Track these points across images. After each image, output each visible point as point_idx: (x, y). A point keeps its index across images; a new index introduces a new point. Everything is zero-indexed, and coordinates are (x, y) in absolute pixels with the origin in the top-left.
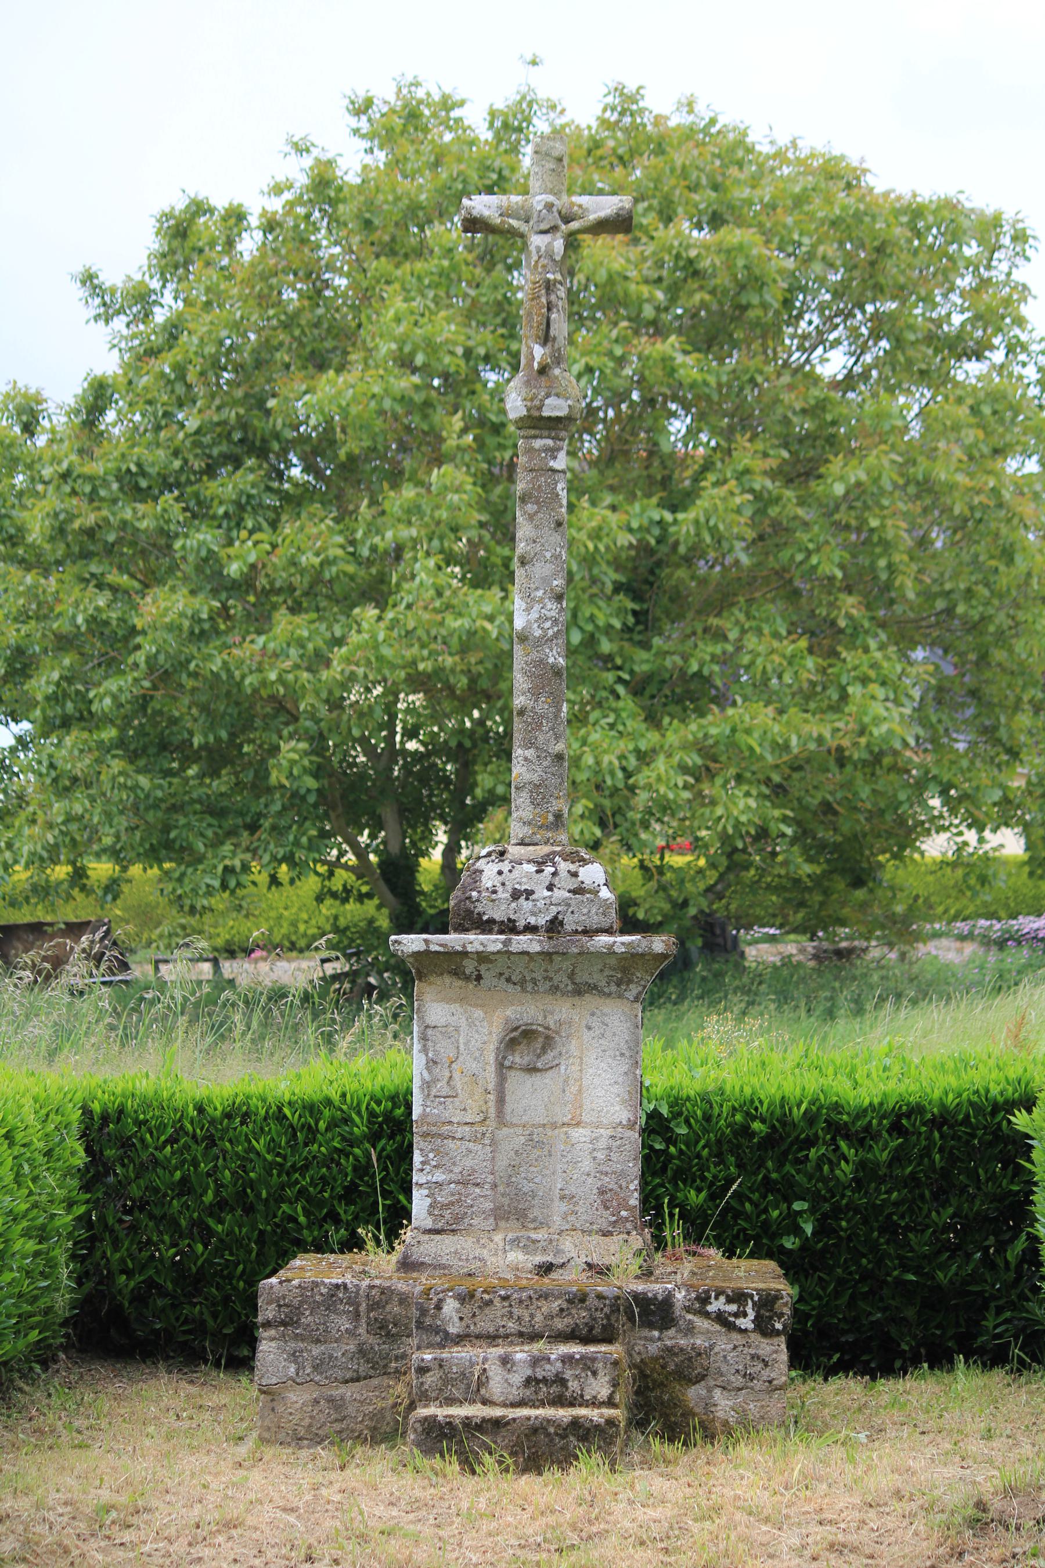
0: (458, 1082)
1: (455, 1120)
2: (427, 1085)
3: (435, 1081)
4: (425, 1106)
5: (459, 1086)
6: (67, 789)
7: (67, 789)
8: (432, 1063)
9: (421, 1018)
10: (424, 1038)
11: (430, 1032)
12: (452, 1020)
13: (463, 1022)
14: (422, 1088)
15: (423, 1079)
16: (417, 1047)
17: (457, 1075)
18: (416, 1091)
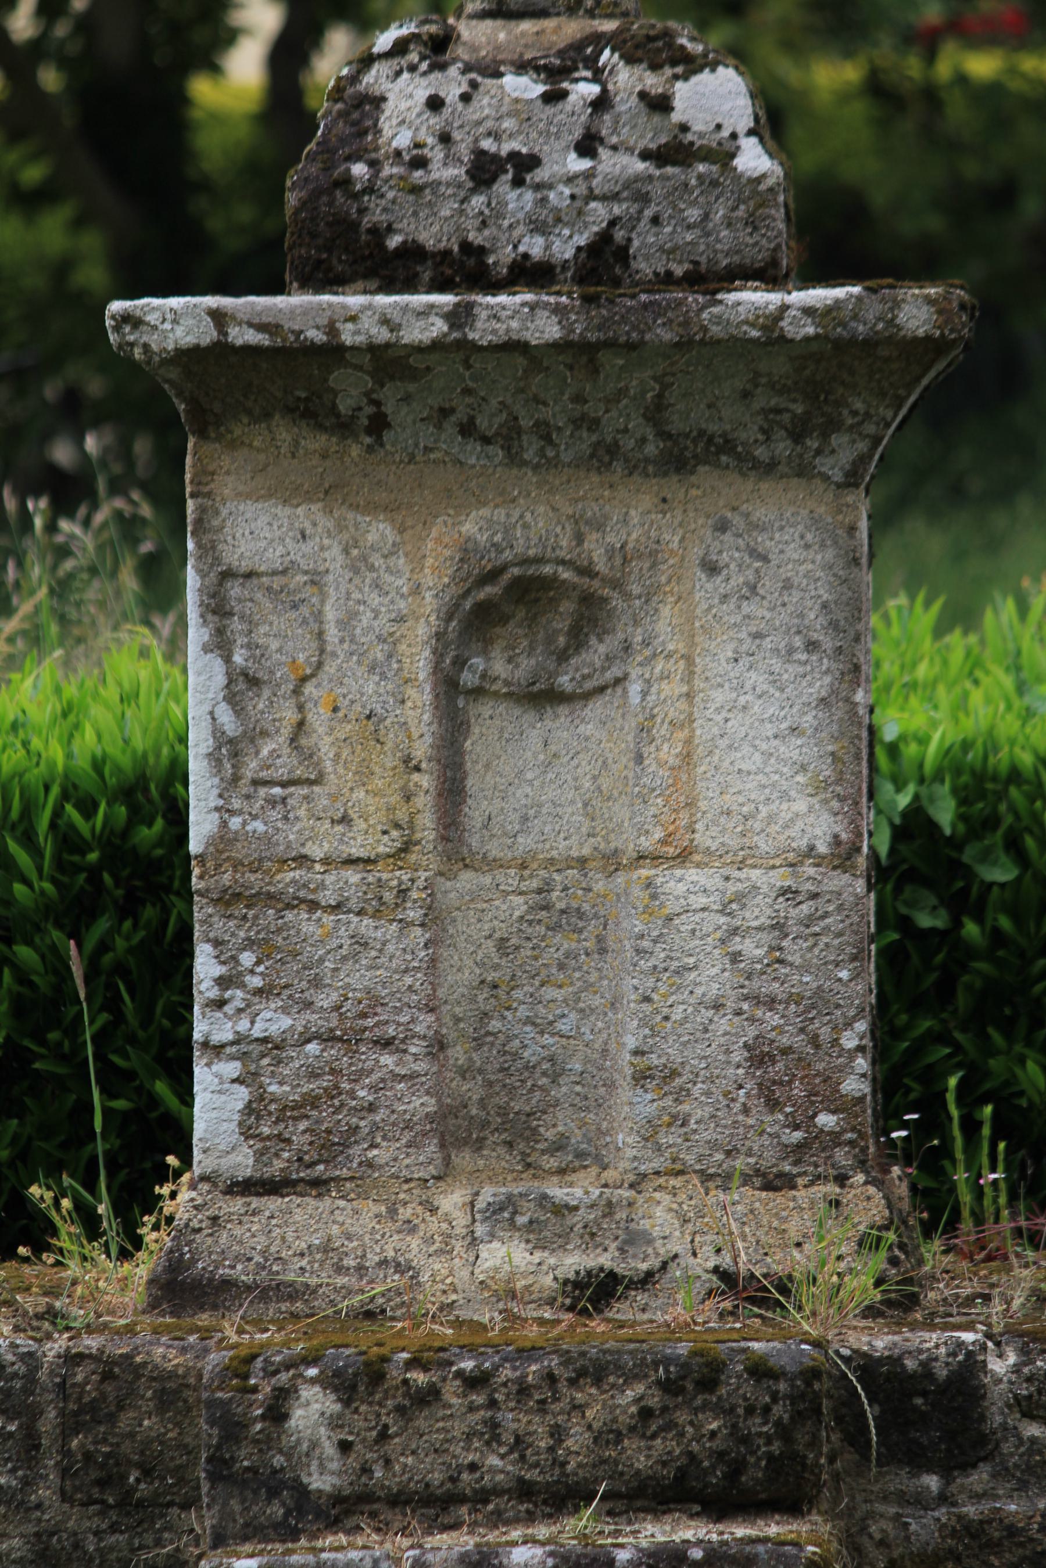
0: (323, 739)
2: (230, 750)
4: (225, 811)
5: (326, 750)
8: (242, 685)
9: (208, 550)
10: (217, 609)
11: (235, 590)
12: (302, 553)
13: (334, 558)
14: (214, 758)
15: (217, 732)
16: (196, 635)
17: (319, 718)
18: (197, 767)
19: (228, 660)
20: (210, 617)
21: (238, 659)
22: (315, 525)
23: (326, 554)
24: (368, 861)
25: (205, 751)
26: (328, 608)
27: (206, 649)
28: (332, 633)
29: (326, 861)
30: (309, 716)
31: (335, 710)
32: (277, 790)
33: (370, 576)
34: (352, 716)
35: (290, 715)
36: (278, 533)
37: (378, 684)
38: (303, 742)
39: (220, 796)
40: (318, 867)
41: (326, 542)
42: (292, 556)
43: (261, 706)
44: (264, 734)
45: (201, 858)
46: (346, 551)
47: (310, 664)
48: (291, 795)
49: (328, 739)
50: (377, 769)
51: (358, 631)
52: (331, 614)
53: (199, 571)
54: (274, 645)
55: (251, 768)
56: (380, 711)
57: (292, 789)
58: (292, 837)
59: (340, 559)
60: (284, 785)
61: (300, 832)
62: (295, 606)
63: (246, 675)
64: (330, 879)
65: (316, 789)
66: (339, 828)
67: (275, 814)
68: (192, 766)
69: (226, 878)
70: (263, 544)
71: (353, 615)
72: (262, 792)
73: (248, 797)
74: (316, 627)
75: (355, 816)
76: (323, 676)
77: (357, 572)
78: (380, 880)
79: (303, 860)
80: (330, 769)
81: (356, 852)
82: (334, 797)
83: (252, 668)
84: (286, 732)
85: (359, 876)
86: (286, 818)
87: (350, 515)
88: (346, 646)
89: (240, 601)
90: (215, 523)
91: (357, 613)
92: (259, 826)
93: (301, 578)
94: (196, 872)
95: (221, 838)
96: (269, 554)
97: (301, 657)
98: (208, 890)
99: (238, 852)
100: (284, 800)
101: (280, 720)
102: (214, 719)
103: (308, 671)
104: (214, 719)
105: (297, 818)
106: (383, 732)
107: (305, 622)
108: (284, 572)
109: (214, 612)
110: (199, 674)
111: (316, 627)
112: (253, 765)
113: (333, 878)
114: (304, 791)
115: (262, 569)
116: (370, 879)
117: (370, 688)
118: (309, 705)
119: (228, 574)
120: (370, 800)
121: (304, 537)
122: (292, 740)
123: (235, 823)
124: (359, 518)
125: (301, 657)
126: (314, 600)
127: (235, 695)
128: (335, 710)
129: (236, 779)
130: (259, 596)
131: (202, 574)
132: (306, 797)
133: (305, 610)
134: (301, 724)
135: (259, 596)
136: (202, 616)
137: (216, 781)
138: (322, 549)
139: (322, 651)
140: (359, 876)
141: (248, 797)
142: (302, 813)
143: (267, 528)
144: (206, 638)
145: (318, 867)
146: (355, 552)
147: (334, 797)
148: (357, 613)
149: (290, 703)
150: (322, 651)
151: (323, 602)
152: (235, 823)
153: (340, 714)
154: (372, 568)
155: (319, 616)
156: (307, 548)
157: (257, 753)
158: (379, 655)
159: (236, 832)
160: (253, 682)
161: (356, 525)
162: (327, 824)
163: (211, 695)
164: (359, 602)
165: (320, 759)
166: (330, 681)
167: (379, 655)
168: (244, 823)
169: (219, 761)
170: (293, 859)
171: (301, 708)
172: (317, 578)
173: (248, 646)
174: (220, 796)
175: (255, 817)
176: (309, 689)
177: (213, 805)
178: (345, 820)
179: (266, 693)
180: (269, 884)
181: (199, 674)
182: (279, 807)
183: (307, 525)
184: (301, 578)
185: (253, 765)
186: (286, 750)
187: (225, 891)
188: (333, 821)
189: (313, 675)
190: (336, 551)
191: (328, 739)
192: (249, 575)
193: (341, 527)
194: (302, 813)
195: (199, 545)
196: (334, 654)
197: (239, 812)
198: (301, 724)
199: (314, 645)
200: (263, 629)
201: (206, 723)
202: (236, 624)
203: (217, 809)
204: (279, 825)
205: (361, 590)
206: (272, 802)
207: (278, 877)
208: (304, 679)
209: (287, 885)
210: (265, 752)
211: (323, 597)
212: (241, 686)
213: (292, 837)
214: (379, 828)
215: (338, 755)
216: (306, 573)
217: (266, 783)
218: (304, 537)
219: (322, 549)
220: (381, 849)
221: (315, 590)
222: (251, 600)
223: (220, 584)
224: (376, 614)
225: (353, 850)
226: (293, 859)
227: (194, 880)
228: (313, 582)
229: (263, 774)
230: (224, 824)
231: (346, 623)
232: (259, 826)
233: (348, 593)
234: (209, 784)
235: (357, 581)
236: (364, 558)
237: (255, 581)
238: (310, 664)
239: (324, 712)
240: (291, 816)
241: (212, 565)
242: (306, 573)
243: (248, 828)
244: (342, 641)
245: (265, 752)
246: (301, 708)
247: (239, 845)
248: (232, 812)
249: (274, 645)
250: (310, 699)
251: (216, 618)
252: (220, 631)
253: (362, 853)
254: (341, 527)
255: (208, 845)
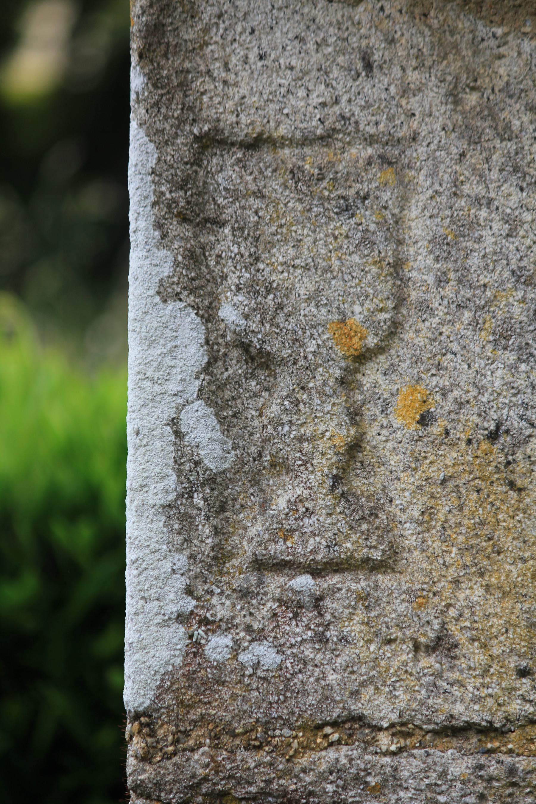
0: (399, 479)
1: (381, 708)
2: (208, 498)
3: (259, 467)
4: (197, 622)
5: (405, 500)
6: (305, 140)
7: (305, 140)
8: (238, 366)
9: (172, 89)
10: (191, 212)
11: (226, 173)
12: (364, 100)
13: (430, 110)
14: (177, 514)
15: (186, 462)
16: (146, 262)
17: (390, 436)
18: (142, 531)
19: (209, 315)
20: (175, 228)
21: (229, 313)
22: (392, 42)
23: (413, 103)
24: (488, 731)
25: (160, 500)
26: (414, 213)
27: (165, 293)
28: (421, 265)
29: (402, 729)
30: (372, 431)
31: (425, 420)
32: (303, 582)
33: (503, 148)
34: (459, 433)
35: (333, 430)
36: (315, 58)
37: (513, 368)
38: (358, 484)
39: (189, 591)
40: (385, 741)
41: (413, 76)
42: (344, 107)
43: (274, 410)
44: (279, 465)
45: (147, 719)
46: (454, 97)
47: (376, 327)
48: (334, 591)
49: (409, 480)
50: (508, 542)
51: (475, 261)
52: (419, 226)
53: (153, 133)
54: (304, 287)
55: (252, 534)
56: (516, 423)
57: (335, 579)
58: (332, 678)
59: (442, 113)
60: (316, 571)
61: (349, 669)
62: (347, 209)
63: (245, 347)
64: (409, 766)
65: (384, 580)
66: (429, 662)
67: (298, 631)
68: (134, 528)
69: (198, 761)
70: (286, 79)
71: (466, 228)
72: (274, 583)
73: (245, 594)
74: (388, 251)
75: (461, 638)
76: (400, 351)
77: (475, 139)
78: (512, 771)
79: (354, 726)
80: (412, 541)
81: (463, 712)
82: (419, 598)
83: (259, 332)
84: (324, 463)
85: (470, 761)
86: (321, 639)
87: (464, 24)
88: (449, 291)
89: (236, 195)
90: (189, 34)
91: (474, 224)
92: (265, 654)
93: (361, 152)
94: (136, 746)
95: (190, 677)
96: (296, 102)
97: (358, 313)
98: (158, 785)
99: (225, 706)
100: (318, 601)
101: (312, 439)
102: (178, 434)
103: (372, 341)
104: (178, 434)
105: (344, 639)
106: (522, 467)
107: (367, 241)
108: (325, 139)
109: (184, 219)
110: (151, 343)
111: (388, 251)
112: (256, 529)
113: (416, 764)
114: (359, 583)
115: (283, 130)
116: (493, 769)
117: (498, 378)
118: (372, 410)
119: (212, 142)
120: (494, 605)
121: (368, 66)
122: (337, 480)
123: (218, 646)
124: (482, 30)
125: (358, 313)
126: (385, 196)
127: (221, 387)
128: (425, 420)
129: (221, 556)
130: (274, 185)
131: (160, 139)
132: (363, 597)
133: (367, 217)
134: (355, 447)
135: (274, 185)
136: (158, 226)
137: (181, 560)
138: (405, 92)
139: (400, 301)
140: (470, 761)
141: (245, 594)
142: (354, 628)
143: (293, 47)
144: (167, 270)
145: (385, 741)
146: (472, 99)
147: (419, 598)
148: (474, 224)
149: (336, 405)
150: (400, 301)
151: (404, 201)
152: (218, 646)
153: (436, 430)
154: (506, 133)
155: (394, 229)
156: (374, 89)
157: (265, 505)
158: (516, 310)
159: (220, 666)
160: (260, 361)
161: (475, 44)
162: (405, 654)
163: (173, 387)
164: (478, 201)
165: (391, 518)
166: (417, 361)
167: (516, 310)
168: (237, 648)
169: (187, 520)
170: (335, 724)
171: (354, 415)
172: (393, 152)
173: (251, 289)
174: (189, 591)
175: (258, 636)
176: (372, 376)
177: (172, 609)
178: (442, 645)
179: (285, 383)
180: (286, 773)
181: (151, 343)
182: (308, 616)
183: (376, 41)
184: (361, 152)
185: (256, 529)
186: (324, 501)
187: (195, 788)
188: (417, 647)
189: (380, 350)
190: (433, 97)
191: (409, 480)
192: (256, 143)
193: (444, 49)
194: (354, 628)
195: (154, 80)
196: (425, 308)
197: (228, 625)
198: (355, 447)
199: (385, 288)
200: (283, 253)
201: (162, 444)
202: (226, 243)
203: (182, 618)
204: (308, 653)
205: (482, 178)
206: (293, 606)
207: (304, 761)
208: (362, 357)
209: (322, 777)
210: (281, 503)
211: (405, 191)
212: (235, 368)
213: (332, 678)
214: (513, 662)
215: (428, 512)
216: (371, 140)
217: (282, 566)
218: (368, 66)
219: (405, 91)
220: (515, 707)
221: (389, 175)
222: (260, 195)
223: (197, 162)
224: (513, 226)
225: (459, 708)
226: (335, 724)
227: (131, 762)
228: (384, 160)
229: (278, 548)
230: (195, 648)
231: (444, 247)
232: (265, 654)
233: (456, 183)
234: (167, 566)
235: (475, 158)
236: (490, 112)
237: (267, 156)
238: (376, 327)
239: (403, 423)
240: (332, 634)
241: (181, 121)
242: (371, 140)
243: (244, 657)
244: (441, 281)
245: (281, 503)
246: (354, 415)
247: (225, 693)
248: (210, 625)
249: (304, 287)
250: (375, 397)
251: (187, 230)
252: (194, 258)
253: (477, 715)
254: (444, 49)
255: (162, 691)
